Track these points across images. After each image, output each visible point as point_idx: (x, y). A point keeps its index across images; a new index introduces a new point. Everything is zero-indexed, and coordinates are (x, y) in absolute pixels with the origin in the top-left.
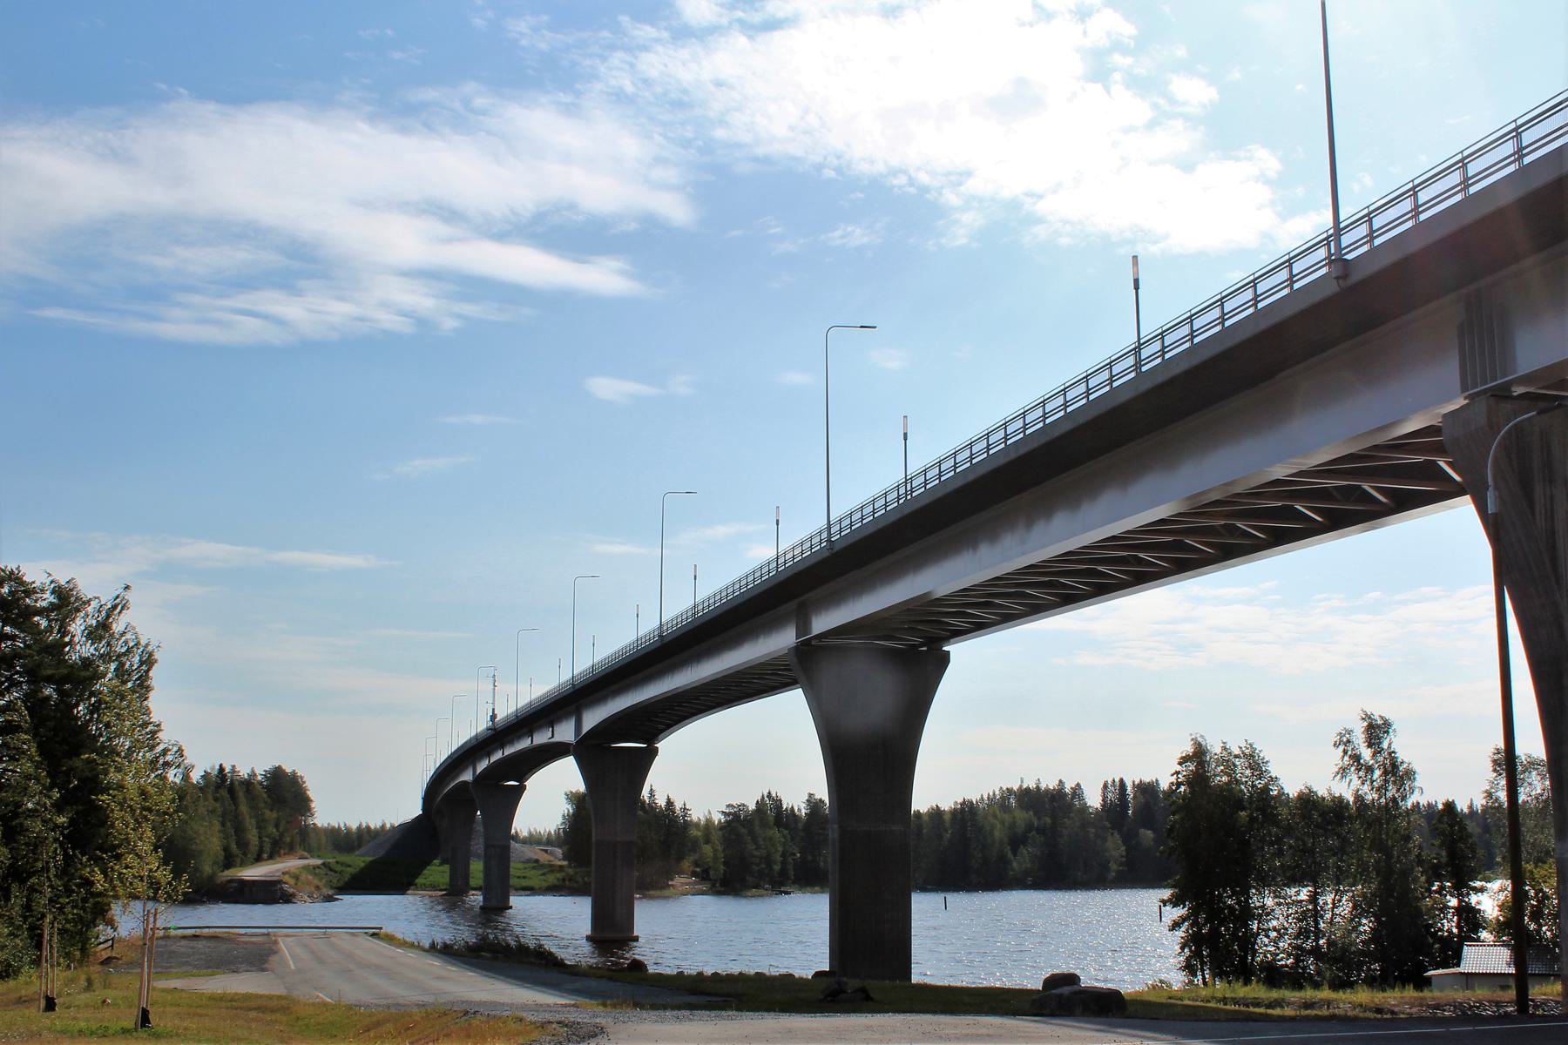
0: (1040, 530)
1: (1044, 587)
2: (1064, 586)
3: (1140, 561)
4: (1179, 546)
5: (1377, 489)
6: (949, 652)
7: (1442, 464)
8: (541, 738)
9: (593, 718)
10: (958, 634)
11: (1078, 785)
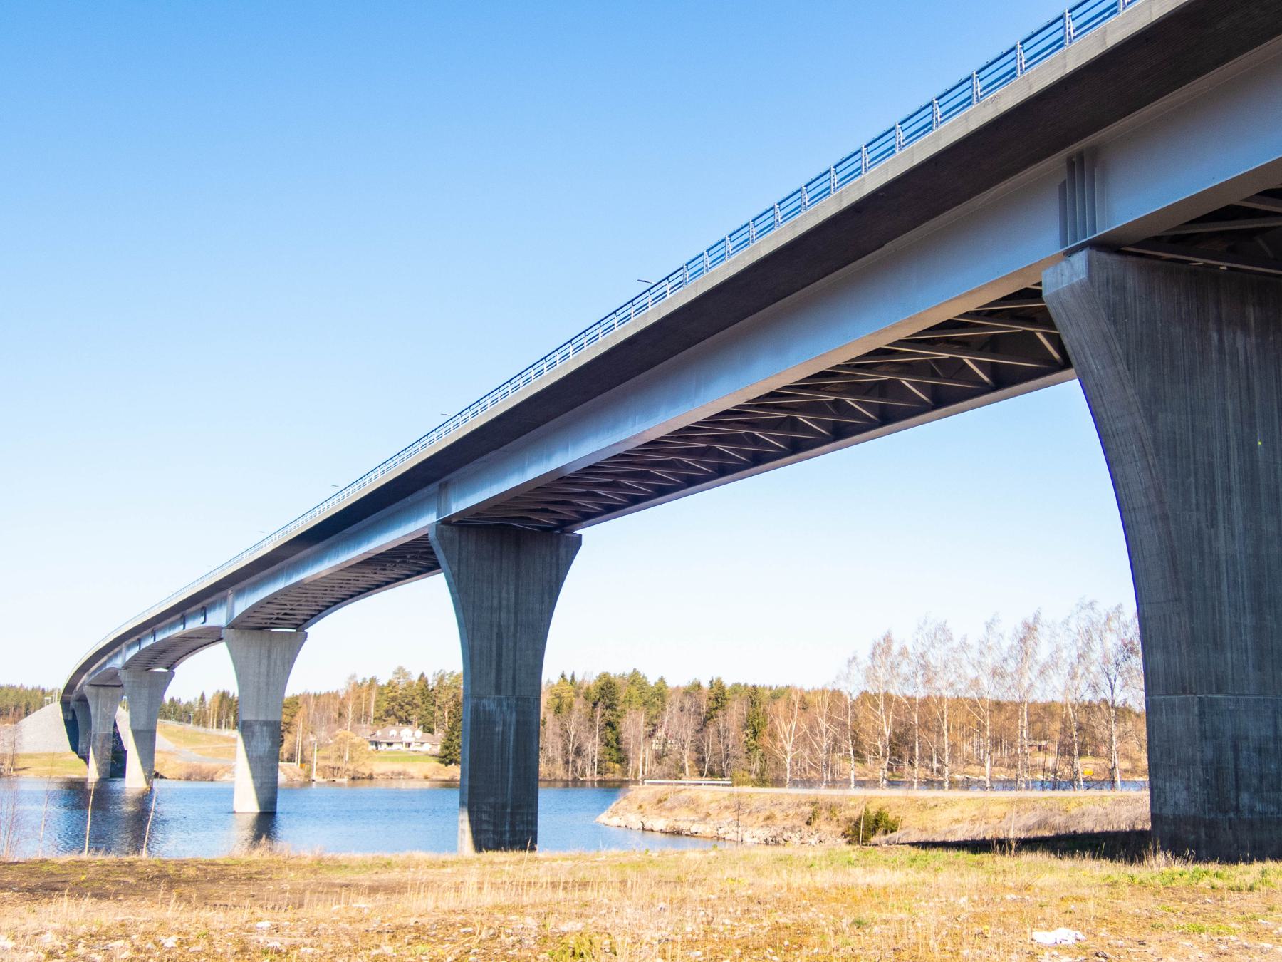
0: (549, 457)
1: (776, 428)
2: (688, 466)
3: (757, 441)
4: (882, 389)
5: (974, 362)
6: (580, 536)
7: (903, 382)
8: (194, 624)
9: (242, 605)
10: (588, 517)
11: (662, 679)
